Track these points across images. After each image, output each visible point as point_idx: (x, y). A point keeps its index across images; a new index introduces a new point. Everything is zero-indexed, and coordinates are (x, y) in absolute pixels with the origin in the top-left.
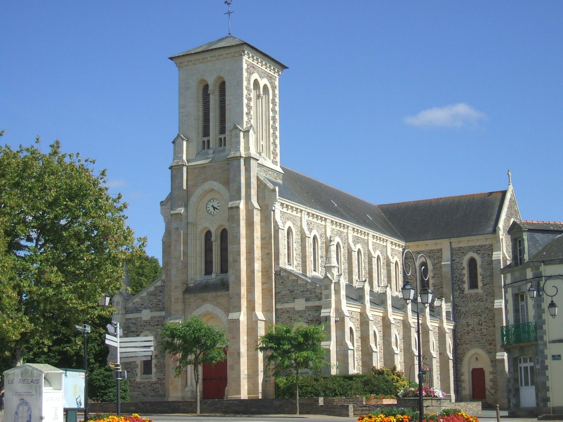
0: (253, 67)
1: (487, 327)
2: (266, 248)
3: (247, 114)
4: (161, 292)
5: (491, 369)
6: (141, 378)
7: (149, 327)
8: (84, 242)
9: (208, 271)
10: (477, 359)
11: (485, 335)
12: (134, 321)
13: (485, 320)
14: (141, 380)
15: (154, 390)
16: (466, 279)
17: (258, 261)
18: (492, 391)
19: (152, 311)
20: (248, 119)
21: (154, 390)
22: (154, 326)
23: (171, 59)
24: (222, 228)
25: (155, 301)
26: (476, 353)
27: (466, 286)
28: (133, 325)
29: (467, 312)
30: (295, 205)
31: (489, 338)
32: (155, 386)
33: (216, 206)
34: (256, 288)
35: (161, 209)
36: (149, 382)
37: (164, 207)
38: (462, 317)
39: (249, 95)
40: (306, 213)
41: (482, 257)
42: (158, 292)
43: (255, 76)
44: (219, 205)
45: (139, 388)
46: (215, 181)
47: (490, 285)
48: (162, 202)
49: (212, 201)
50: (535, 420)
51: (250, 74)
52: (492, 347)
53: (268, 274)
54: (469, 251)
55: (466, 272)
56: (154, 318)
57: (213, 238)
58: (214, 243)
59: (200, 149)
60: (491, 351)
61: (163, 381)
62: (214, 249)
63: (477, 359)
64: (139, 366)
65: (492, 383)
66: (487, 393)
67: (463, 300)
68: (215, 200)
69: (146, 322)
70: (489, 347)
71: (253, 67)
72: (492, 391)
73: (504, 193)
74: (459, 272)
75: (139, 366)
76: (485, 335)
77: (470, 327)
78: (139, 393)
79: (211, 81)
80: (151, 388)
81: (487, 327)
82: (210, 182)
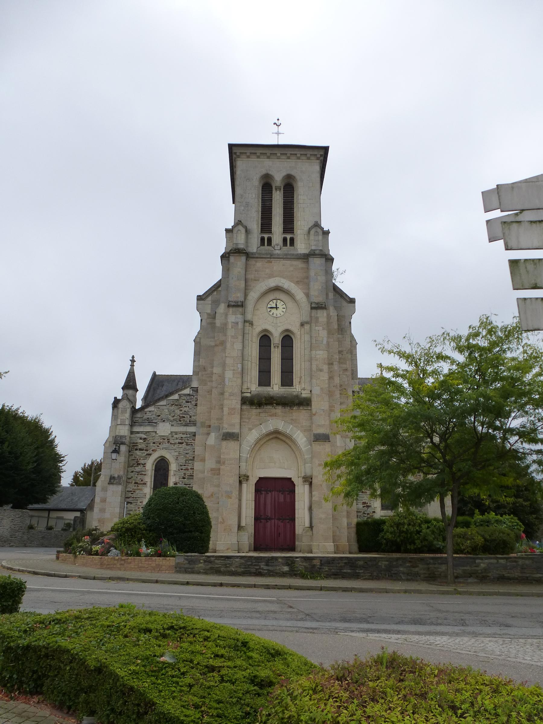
4: (187, 402)
7: (166, 445)
8: (510, 415)
9: (264, 378)
12: (144, 436)
19: (172, 425)
22: (175, 444)
25: (178, 412)
28: (141, 441)
34: (296, 502)
42: (184, 401)
46: (284, 278)
49: (284, 306)
50: (197, 328)
56: (176, 433)
59: (259, 245)
61: (434, 338)
69: (163, 438)
79: (278, 178)
82: (276, 278)
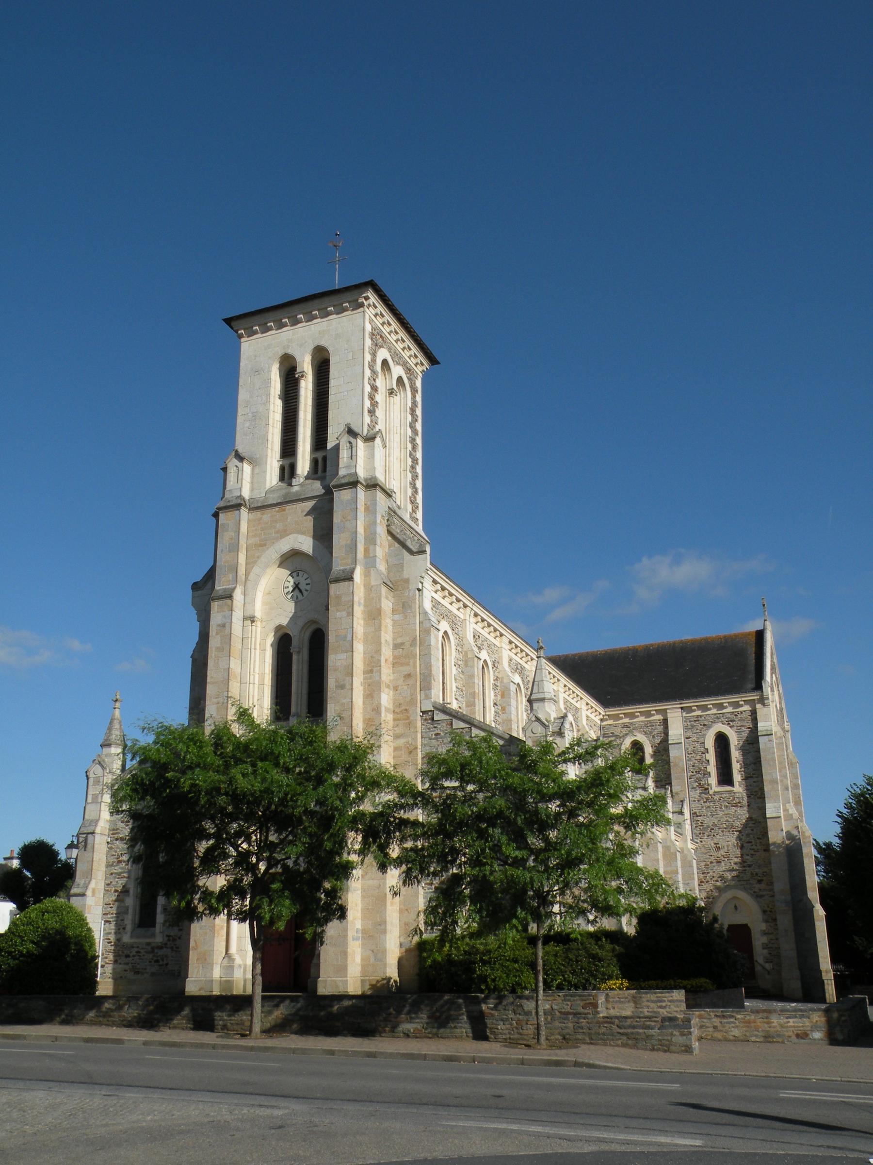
0: (381, 336)
1: (752, 852)
2: (402, 665)
3: (369, 412)
5: (763, 926)
6: (131, 937)
10: (736, 908)
11: (750, 866)
13: (748, 839)
14: (133, 941)
15: (157, 961)
16: (712, 768)
17: (387, 690)
18: (768, 966)
20: (372, 421)
21: (157, 961)
23: (228, 321)
24: (314, 627)
26: (734, 898)
27: (713, 780)
29: (714, 825)
30: (457, 593)
31: (757, 870)
32: (160, 952)
33: (302, 586)
35: (193, 597)
36: (148, 944)
37: (199, 593)
38: (707, 834)
39: (374, 380)
40: (473, 613)
41: (738, 732)
43: (383, 354)
44: (309, 581)
45: (127, 956)
47: (755, 780)
48: (195, 584)
51: (376, 346)
52: (763, 886)
53: (408, 718)
54: (714, 722)
55: (711, 756)
57: (293, 649)
58: (295, 657)
60: (761, 893)
62: (294, 667)
63: (736, 908)
64: (130, 911)
65: (765, 951)
66: (758, 968)
67: (708, 804)
68: (301, 573)
70: (758, 886)
71: (381, 336)
72: (768, 966)
73: (760, 636)
74: (698, 757)
75: (130, 911)
76: (750, 866)
77: (722, 852)
78: (127, 967)
80: (151, 956)
81: (752, 852)
82: (291, 536)
